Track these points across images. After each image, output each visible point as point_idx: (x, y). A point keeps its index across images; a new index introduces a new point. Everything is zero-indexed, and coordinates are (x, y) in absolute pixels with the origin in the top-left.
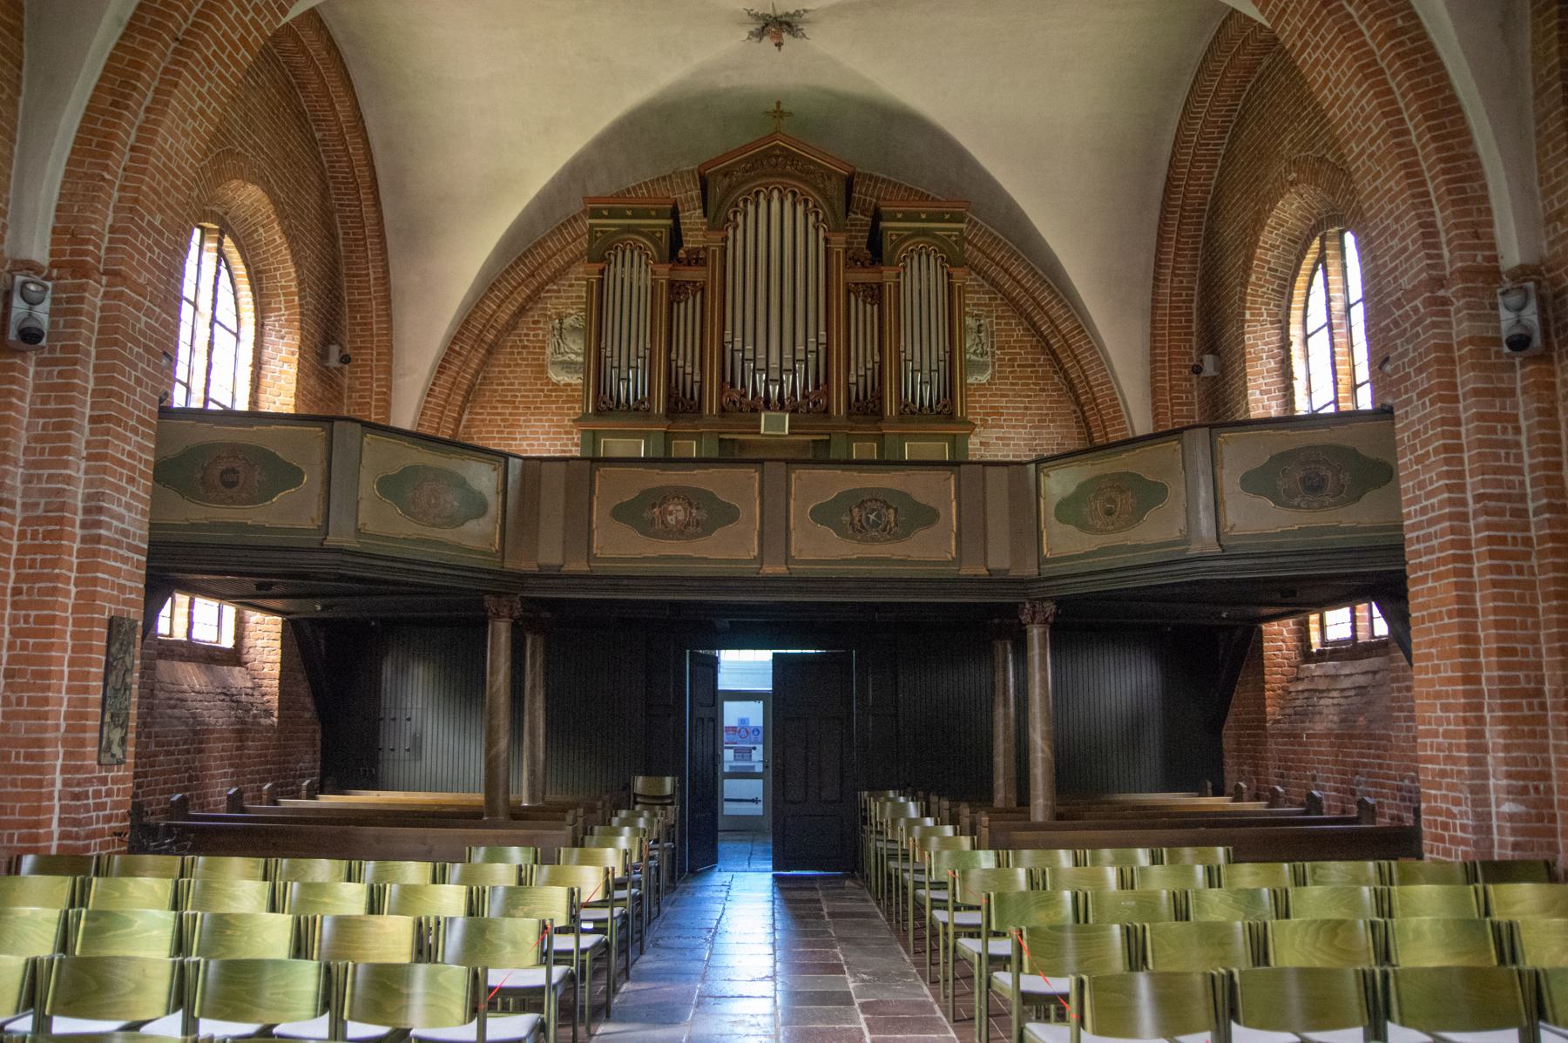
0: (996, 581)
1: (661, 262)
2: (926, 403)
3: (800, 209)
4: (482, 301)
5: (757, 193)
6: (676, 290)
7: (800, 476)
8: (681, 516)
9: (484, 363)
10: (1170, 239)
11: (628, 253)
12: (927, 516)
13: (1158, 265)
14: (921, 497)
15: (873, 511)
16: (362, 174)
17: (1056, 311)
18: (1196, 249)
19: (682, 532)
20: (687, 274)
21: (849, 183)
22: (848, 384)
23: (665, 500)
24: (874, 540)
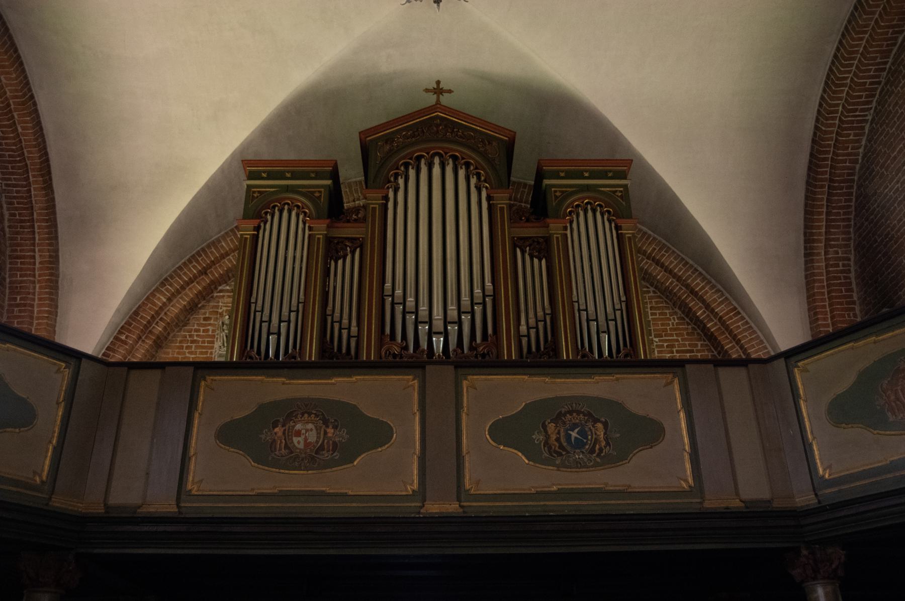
1: (318, 218)
3: (462, 173)
4: (153, 294)
6: (334, 249)
7: (476, 383)
8: (312, 437)
10: (820, 213)
11: (285, 214)
12: (650, 432)
13: (809, 240)
14: (636, 406)
16: (32, 156)
17: (710, 296)
18: (849, 220)
19: (313, 459)
20: (347, 231)
22: (519, 337)
23: (290, 417)
24: (579, 465)
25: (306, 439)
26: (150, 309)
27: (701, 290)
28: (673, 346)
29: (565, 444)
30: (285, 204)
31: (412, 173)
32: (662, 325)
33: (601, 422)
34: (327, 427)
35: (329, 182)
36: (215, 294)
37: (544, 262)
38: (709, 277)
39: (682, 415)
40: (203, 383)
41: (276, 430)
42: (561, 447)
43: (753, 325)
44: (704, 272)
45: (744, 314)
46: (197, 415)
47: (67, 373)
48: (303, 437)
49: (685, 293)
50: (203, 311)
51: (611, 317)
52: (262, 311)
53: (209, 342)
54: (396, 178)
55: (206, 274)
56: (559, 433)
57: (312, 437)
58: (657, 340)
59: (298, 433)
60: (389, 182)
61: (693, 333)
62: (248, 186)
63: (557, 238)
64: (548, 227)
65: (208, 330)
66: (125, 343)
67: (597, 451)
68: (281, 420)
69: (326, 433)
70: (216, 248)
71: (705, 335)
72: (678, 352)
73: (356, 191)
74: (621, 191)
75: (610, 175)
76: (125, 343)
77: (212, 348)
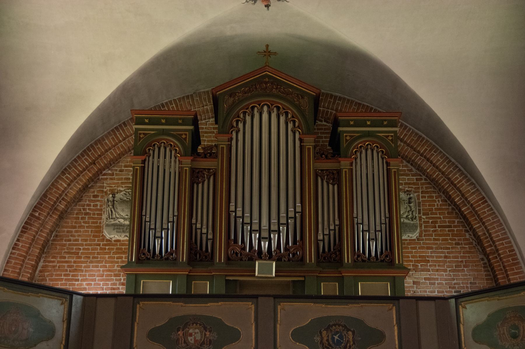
1: (186, 155)
2: (373, 254)
3: (282, 119)
4: (56, 181)
6: (196, 175)
7: (285, 308)
8: (198, 337)
9: (57, 225)
11: (162, 149)
14: (371, 322)
15: (337, 333)
17: (465, 187)
21: (316, 101)
22: (317, 241)
23: (186, 325)
25: (195, 338)
26: (55, 192)
27: (458, 183)
28: (436, 222)
29: (331, 343)
30: (161, 143)
31: (248, 119)
32: (429, 205)
33: (351, 331)
34: (206, 331)
35: (192, 127)
36: (101, 177)
37: (336, 186)
38: (466, 173)
39: (396, 328)
40: (138, 306)
41: (179, 333)
42: (329, 344)
43: (496, 211)
44: (462, 169)
45: (489, 202)
46: (136, 324)
48: (193, 337)
49: (447, 183)
50: (92, 190)
51: (383, 222)
52: (150, 222)
53: (98, 214)
54: (237, 124)
55: (94, 164)
56: (328, 337)
58: (424, 217)
59: (191, 335)
60: (233, 127)
61: (452, 212)
62: (136, 129)
63: (346, 172)
64: (340, 162)
65: (97, 205)
66: (38, 218)
67: (348, 347)
68: (181, 327)
69: (205, 335)
70: (102, 145)
71: (462, 215)
72: (439, 227)
73: (205, 100)
74: (392, 136)
75: (385, 123)
76: (38, 218)
77: (101, 219)
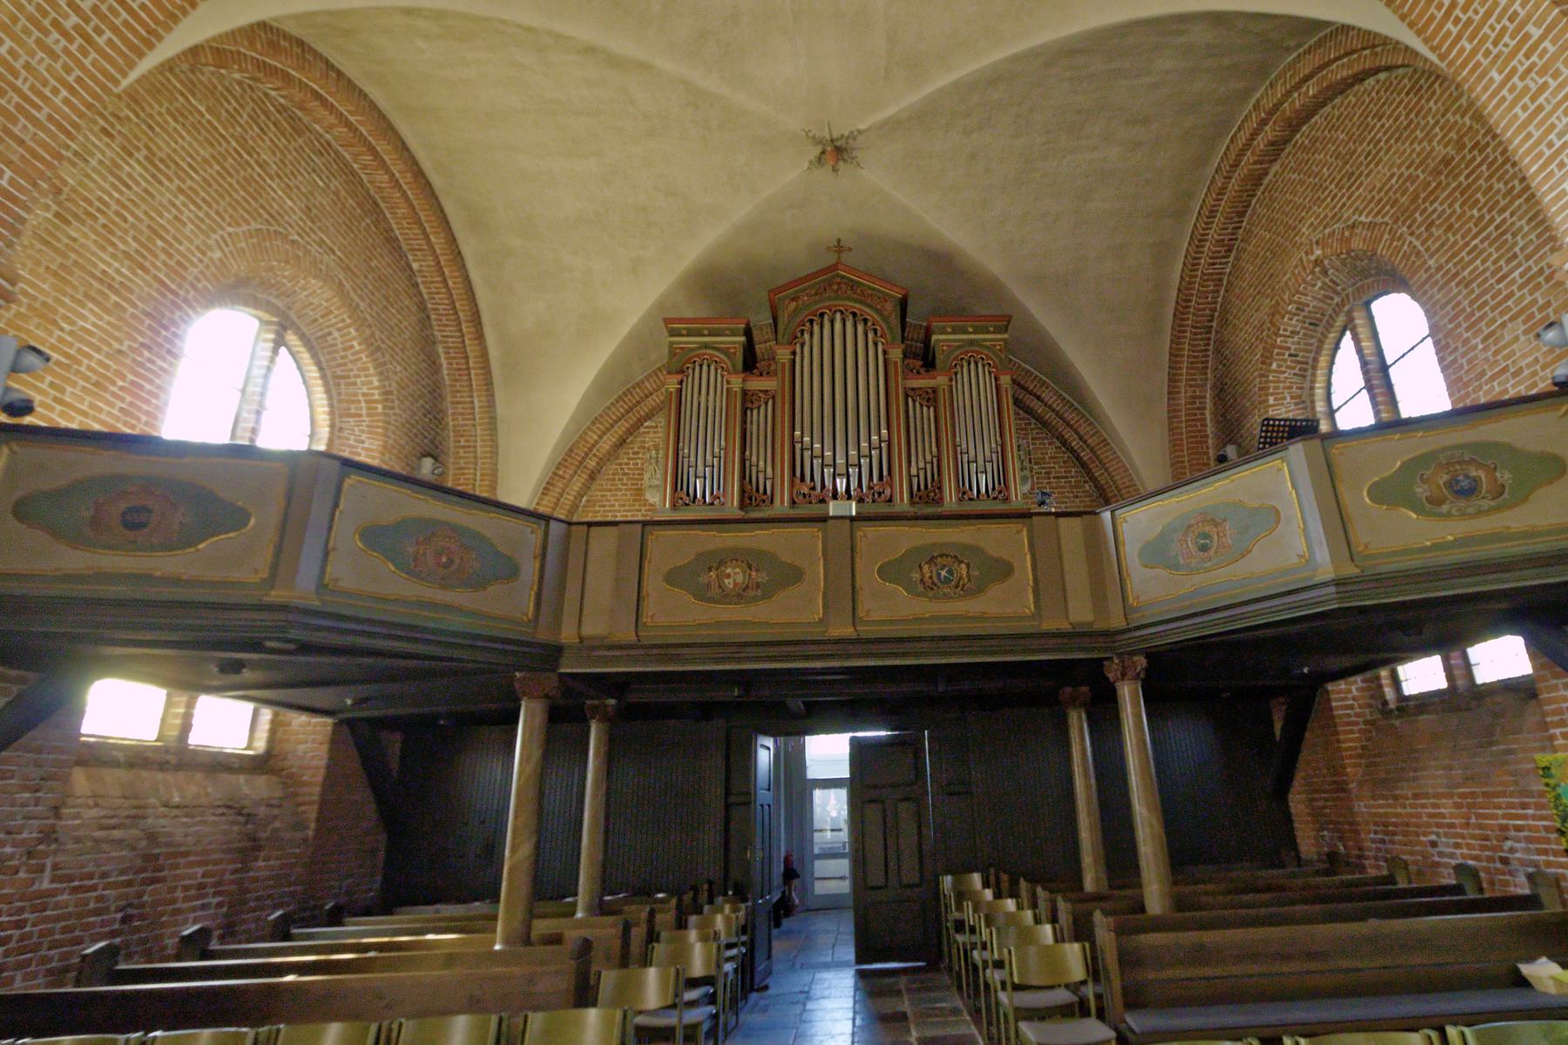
0: (1078, 635)
1: (736, 372)
2: (983, 490)
5: (822, 315)
8: (740, 579)
9: (586, 488)
11: (705, 368)
12: (1003, 570)
14: (993, 550)
15: (944, 566)
19: (741, 596)
21: (903, 304)
23: (721, 563)
24: (947, 597)
47: (540, 533)
57: (740, 579)
59: (728, 576)
